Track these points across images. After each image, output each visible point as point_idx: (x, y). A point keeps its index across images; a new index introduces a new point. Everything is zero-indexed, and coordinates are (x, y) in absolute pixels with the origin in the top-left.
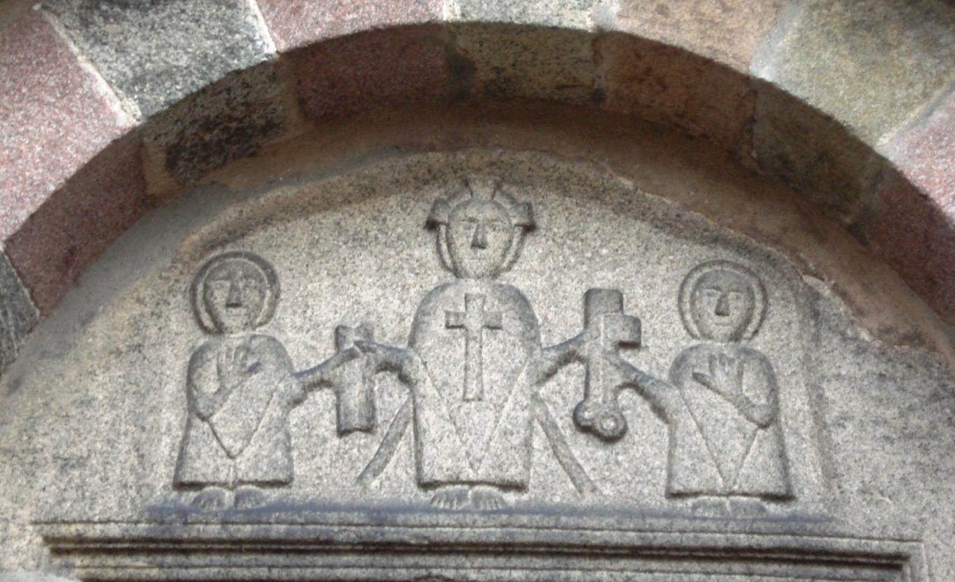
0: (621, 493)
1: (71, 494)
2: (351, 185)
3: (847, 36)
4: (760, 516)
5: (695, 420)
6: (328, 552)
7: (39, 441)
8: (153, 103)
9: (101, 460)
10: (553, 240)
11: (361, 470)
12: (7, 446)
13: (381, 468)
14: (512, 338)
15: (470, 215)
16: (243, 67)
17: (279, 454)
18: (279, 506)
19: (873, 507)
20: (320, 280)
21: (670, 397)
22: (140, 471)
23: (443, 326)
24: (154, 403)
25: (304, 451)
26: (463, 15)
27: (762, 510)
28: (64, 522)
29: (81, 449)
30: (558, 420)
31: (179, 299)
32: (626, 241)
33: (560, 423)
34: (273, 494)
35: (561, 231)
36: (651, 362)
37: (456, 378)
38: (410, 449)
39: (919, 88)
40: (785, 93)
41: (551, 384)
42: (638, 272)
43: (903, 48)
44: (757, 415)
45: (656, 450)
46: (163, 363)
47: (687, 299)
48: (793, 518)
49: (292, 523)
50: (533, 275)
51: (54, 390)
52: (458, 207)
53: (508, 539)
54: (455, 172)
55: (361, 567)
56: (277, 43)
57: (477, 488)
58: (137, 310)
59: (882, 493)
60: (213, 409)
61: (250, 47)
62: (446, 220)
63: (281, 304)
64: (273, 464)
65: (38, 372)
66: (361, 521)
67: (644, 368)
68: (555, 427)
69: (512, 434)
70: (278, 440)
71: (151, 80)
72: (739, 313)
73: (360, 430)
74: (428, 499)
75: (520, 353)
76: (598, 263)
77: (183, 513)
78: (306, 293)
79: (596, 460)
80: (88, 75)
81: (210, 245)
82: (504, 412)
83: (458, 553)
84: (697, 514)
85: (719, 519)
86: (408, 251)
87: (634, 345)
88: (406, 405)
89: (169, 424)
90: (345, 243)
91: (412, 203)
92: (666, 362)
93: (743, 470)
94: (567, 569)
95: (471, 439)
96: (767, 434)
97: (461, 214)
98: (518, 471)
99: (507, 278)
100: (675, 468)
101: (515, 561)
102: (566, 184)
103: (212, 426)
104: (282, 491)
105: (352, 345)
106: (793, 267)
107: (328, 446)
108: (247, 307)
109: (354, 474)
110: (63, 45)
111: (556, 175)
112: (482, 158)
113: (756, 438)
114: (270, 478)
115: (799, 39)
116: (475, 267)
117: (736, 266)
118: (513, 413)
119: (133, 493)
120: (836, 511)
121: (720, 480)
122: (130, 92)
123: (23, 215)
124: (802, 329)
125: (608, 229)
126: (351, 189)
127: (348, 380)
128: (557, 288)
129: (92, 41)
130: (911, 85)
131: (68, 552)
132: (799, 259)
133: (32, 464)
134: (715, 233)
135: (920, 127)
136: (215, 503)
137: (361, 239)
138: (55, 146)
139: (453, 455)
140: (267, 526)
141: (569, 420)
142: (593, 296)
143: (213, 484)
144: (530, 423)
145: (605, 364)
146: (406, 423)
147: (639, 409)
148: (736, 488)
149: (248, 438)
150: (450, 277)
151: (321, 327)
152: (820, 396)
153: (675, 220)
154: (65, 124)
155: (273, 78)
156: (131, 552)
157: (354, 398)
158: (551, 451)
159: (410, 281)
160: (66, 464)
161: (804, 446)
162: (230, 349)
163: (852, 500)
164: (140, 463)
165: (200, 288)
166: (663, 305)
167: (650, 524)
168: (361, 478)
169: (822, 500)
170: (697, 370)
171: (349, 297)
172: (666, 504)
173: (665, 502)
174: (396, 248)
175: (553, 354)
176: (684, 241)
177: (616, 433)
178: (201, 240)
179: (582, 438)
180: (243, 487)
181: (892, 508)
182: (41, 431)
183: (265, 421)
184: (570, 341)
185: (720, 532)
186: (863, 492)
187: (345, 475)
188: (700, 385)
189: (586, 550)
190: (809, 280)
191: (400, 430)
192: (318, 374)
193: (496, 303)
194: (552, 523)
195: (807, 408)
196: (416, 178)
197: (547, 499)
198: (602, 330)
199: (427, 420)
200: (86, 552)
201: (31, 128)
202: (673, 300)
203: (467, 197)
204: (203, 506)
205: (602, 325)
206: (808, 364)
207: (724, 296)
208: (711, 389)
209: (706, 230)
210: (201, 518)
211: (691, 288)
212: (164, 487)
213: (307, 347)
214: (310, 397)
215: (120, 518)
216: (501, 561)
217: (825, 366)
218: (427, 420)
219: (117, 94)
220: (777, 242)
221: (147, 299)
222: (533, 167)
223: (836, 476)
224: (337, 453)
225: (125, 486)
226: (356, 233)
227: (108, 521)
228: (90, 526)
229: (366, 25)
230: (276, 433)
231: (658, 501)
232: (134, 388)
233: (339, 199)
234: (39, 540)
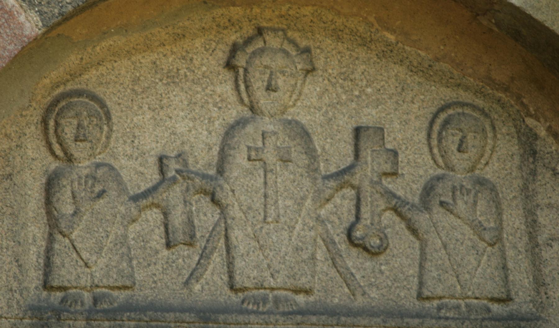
0: (384, 296)
4: (487, 316)
5: (441, 239)
8: (50, 15)
10: (329, 80)
11: (186, 276)
14: (300, 170)
15: (265, 63)
17: (125, 264)
20: (143, 114)
21: (422, 220)
22: (20, 277)
23: (246, 159)
25: (142, 260)
27: (489, 310)
30: (335, 236)
32: (387, 82)
33: (337, 239)
35: (335, 71)
37: (258, 205)
38: (222, 259)
40: (530, 17)
42: (396, 109)
44: (487, 237)
47: (435, 136)
49: (140, 320)
50: (312, 110)
52: (254, 53)
54: (250, 21)
57: (276, 292)
63: (114, 135)
64: (120, 272)
68: (334, 243)
69: (302, 250)
70: (123, 253)
72: (475, 151)
74: (239, 300)
75: (307, 183)
76: (364, 100)
78: (132, 125)
79: (365, 270)
82: (295, 233)
84: (442, 315)
85: (457, 319)
89: (34, 236)
90: (161, 80)
92: (418, 187)
96: (494, 250)
98: (307, 280)
100: (425, 277)
102: (340, 33)
103: (72, 242)
104: (128, 292)
105: (174, 173)
106: (518, 111)
107: (159, 256)
108: (91, 141)
109: (181, 280)
111: (333, 26)
112: (273, 11)
113: (486, 254)
114: (120, 284)
116: (269, 107)
117: (474, 107)
118: (302, 233)
119: (17, 296)
120: (542, 312)
124: (522, 162)
125: (372, 71)
128: (332, 122)
132: (522, 104)
134: (458, 81)
136: (79, 304)
137: (173, 76)
139: (257, 267)
140: (120, 322)
141: (344, 237)
142: (363, 134)
145: (372, 192)
147: (397, 228)
148: (470, 293)
151: (147, 155)
152: (535, 221)
153: (427, 69)
157: (177, 219)
158: (330, 261)
159: (214, 115)
161: (520, 257)
162: (80, 177)
163: (554, 304)
164: (21, 272)
165: (52, 123)
167: (407, 323)
168: (187, 283)
169: (531, 301)
170: (442, 199)
171: (167, 128)
173: (417, 303)
174: (202, 85)
176: (433, 83)
178: (51, 83)
179: (354, 251)
180: (98, 290)
183: (112, 237)
187: (174, 281)
188: (445, 210)
190: (530, 121)
193: (287, 139)
195: (523, 227)
196: (218, 26)
197: (328, 301)
198: (369, 162)
199: (236, 238)
202: (423, 135)
204: (70, 306)
205: (369, 159)
206: (527, 193)
207: (464, 137)
208: (453, 214)
209: (451, 78)
210: (71, 316)
211: (440, 123)
212: (36, 288)
215: (9, 315)
217: (540, 196)
218: (236, 238)
219: (21, 6)
220: (506, 90)
221: (13, 135)
222: (315, 20)
224: (167, 262)
225: (11, 290)
226: (169, 71)
230: (121, 247)
232: (10, 211)
233: (157, 44)
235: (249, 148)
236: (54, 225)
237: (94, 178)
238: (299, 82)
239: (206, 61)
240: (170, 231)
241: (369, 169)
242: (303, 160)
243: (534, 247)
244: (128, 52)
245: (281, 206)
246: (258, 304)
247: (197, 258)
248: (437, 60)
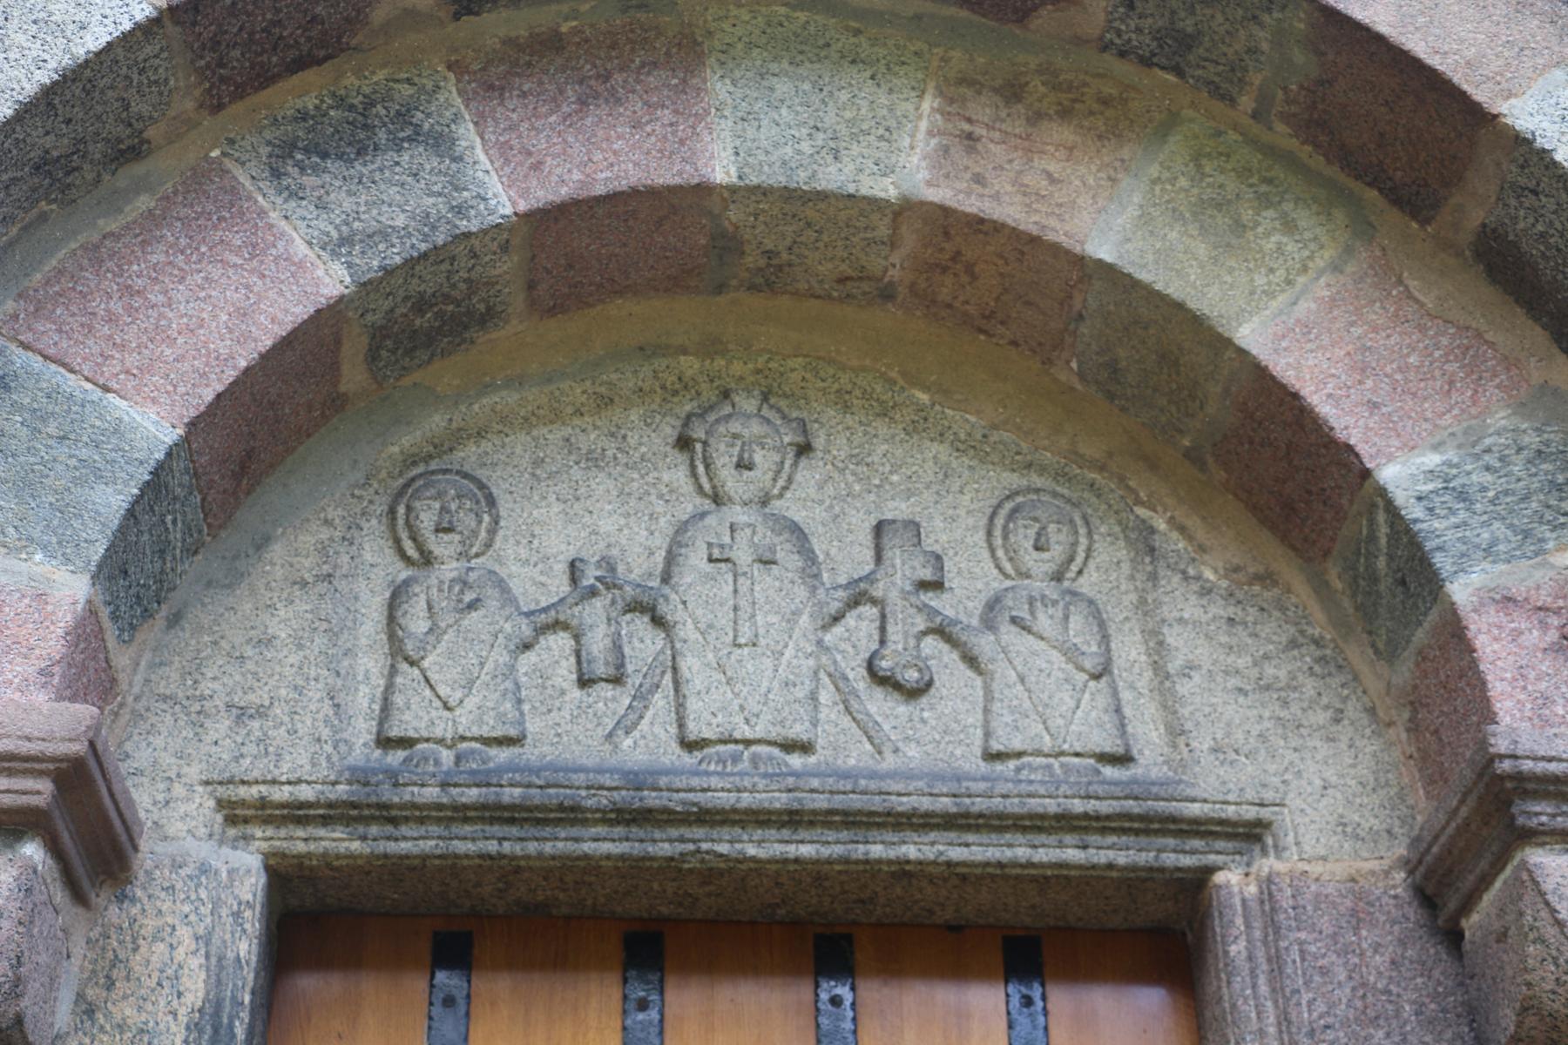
1: (251, 749)
2: (584, 392)
3: (1194, 214)
6: (573, 822)
7: (206, 687)
9: (287, 710)
11: (610, 727)
12: (168, 692)
13: (635, 725)
16: (474, 230)
17: (509, 705)
18: (512, 767)
19: (1226, 767)
20: (549, 506)
21: (984, 644)
24: (349, 645)
26: (740, 177)
27: (1098, 772)
28: (243, 782)
29: (260, 697)
31: (374, 526)
33: (851, 675)
34: (502, 755)
36: (953, 605)
37: (724, 619)
39: (1281, 273)
41: (838, 630)
43: (1260, 230)
44: (1088, 665)
45: (968, 706)
46: (356, 598)
47: (998, 532)
49: (529, 786)
51: (224, 626)
52: (718, 421)
53: (796, 806)
55: (614, 840)
56: (514, 204)
57: (753, 748)
58: (325, 534)
59: (1236, 751)
60: (423, 648)
61: (482, 207)
62: (703, 437)
63: (501, 533)
64: (501, 717)
65: (204, 605)
66: (614, 784)
67: (950, 612)
68: (846, 679)
71: (361, 241)
73: (607, 681)
74: (695, 761)
75: (801, 592)
77: (393, 777)
80: (283, 234)
81: (411, 460)
83: (734, 823)
84: (1022, 777)
86: (656, 474)
87: (937, 585)
88: (662, 651)
90: (577, 463)
91: (658, 417)
92: (976, 606)
93: (1073, 727)
94: (867, 842)
95: (745, 690)
97: (722, 429)
99: (777, 505)
100: (993, 724)
101: (802, 834)
102: (847, 397)
104: (516, 750)
107: (567, 698)
110: (249, 198)
111: (836, 386)
115: (1140, 217)
117: (1055, 495)
118: (795, 661)
119: (328, 748)
120: (1184, 773)
121: (1047, 738)
122: (335, 254)
123: (209, 395)
124: (1134, 568)
125: (899, 452)
126: (584, 398)
127: (590, 621)
129: (286, 194)
130: (1272, 270)
131: (246, 821)
132: (1128, 487)
133: (199, 713)
135: (1284, 318)
138: (245, 315)
142: (886, 528)
143: (427, 740)
144: (816, 673)
146: (663, 673)
147: (946, 659)
148: (1066, 747)
149: (470, 684)
150: (707, 504)
152: (1161, 643)
154: (256, 289)
155: (505, 248)
156: (326, 821)
157: (598, 643)
158: (841, 707)
159: (659, 509)
160: (242, 714)
165: (401, 510)
166: (968, 540)
169: (1165, 762)
170: (1014, 613)
171: (584, 526)
172: (984, 767)
173: (982, 764)
175: (841, 594)
177: (922, 685)
178: (402, 452)
179: (879, 693)
180: (465, 745)
181: (1250, 769)
182: (210, 675)
184: (860, 579)
185: (1050, 797)
186: (1215, 750)
189: (890, 819)
191: (656, 680)
192: (553, 613)
194: (849, 787)
195: (1143, 658)
196: (663, 387)
197: (839, 762)
200: (267, 821)
201: (213, 293)
202: (981, 535)
203: (728, 409)
204: (417, 766)
205: (898, 561)
206: (1144, 607)
207: (1044, 528)
209: (1018, 453)
211: (1001, 519)
212: (364, 745)
213: (535, 583)
214: (541, 639)
215: (314, 778)
216: (786, 833)
220: (1102, 469)
221: (337, 521)
222: (808, 376)
223: (1183, 732)
225: (319, 740)
226: (590, 452)
227: (299, 781)
228: (276, 788)
229: (623, 185)
231: (972, 762)
232: (325, 625)
233: (570, 410)
234: (212, 803)
235: (710, 545)
236: (399, 651)
237: (465, 583)
238: (788, 463)
239: (645, 439)
240: (583, 659)
241: (899, 575)
242: (796, 561)
244: (526, 419)
245: (760, 623)
246: (724, 763)
247: (627, 702)
248: (995, 427)
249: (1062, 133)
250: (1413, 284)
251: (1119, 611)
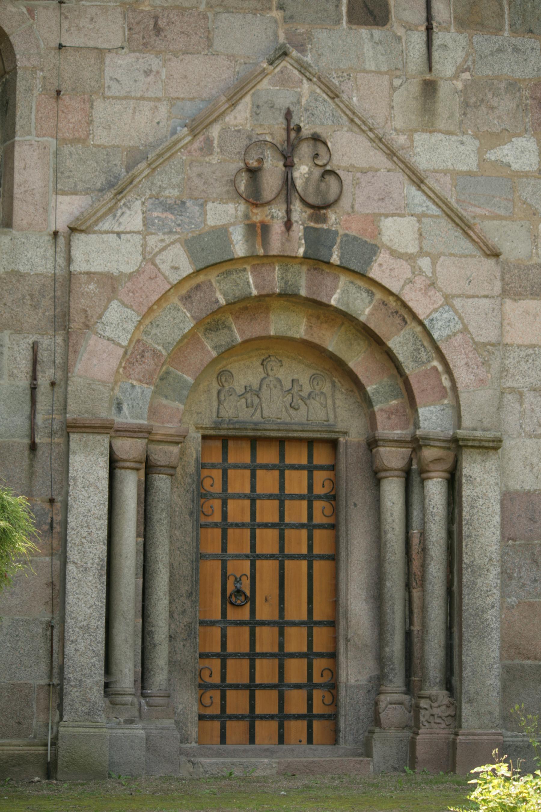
7: (192, 409)
21: (308, 402)
29: (199, 411)
36: (304, 394)
37: (269, 398)
48: (329, 425)
75: (280, 393)
87: (301, 391)
92: (307, 394)
148: (370, 121)
149: (230, 408)
157: (249, 401)
160: (198, 413)
206: (333, 396)
211: (313, 378)
229: (257, 336)
236: (220, 402)
242: (280, 387)
243: (334, 408)
249: (325, 326)
250: (376, 355)
251: (329, 396)
